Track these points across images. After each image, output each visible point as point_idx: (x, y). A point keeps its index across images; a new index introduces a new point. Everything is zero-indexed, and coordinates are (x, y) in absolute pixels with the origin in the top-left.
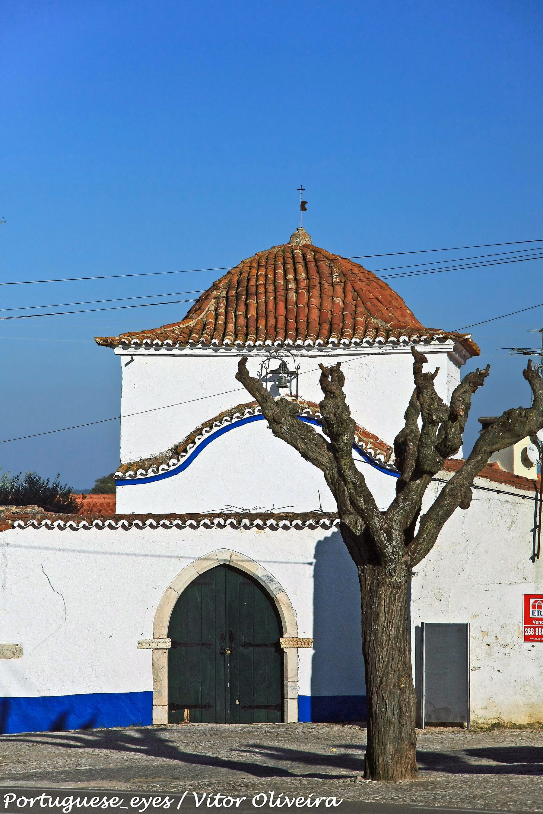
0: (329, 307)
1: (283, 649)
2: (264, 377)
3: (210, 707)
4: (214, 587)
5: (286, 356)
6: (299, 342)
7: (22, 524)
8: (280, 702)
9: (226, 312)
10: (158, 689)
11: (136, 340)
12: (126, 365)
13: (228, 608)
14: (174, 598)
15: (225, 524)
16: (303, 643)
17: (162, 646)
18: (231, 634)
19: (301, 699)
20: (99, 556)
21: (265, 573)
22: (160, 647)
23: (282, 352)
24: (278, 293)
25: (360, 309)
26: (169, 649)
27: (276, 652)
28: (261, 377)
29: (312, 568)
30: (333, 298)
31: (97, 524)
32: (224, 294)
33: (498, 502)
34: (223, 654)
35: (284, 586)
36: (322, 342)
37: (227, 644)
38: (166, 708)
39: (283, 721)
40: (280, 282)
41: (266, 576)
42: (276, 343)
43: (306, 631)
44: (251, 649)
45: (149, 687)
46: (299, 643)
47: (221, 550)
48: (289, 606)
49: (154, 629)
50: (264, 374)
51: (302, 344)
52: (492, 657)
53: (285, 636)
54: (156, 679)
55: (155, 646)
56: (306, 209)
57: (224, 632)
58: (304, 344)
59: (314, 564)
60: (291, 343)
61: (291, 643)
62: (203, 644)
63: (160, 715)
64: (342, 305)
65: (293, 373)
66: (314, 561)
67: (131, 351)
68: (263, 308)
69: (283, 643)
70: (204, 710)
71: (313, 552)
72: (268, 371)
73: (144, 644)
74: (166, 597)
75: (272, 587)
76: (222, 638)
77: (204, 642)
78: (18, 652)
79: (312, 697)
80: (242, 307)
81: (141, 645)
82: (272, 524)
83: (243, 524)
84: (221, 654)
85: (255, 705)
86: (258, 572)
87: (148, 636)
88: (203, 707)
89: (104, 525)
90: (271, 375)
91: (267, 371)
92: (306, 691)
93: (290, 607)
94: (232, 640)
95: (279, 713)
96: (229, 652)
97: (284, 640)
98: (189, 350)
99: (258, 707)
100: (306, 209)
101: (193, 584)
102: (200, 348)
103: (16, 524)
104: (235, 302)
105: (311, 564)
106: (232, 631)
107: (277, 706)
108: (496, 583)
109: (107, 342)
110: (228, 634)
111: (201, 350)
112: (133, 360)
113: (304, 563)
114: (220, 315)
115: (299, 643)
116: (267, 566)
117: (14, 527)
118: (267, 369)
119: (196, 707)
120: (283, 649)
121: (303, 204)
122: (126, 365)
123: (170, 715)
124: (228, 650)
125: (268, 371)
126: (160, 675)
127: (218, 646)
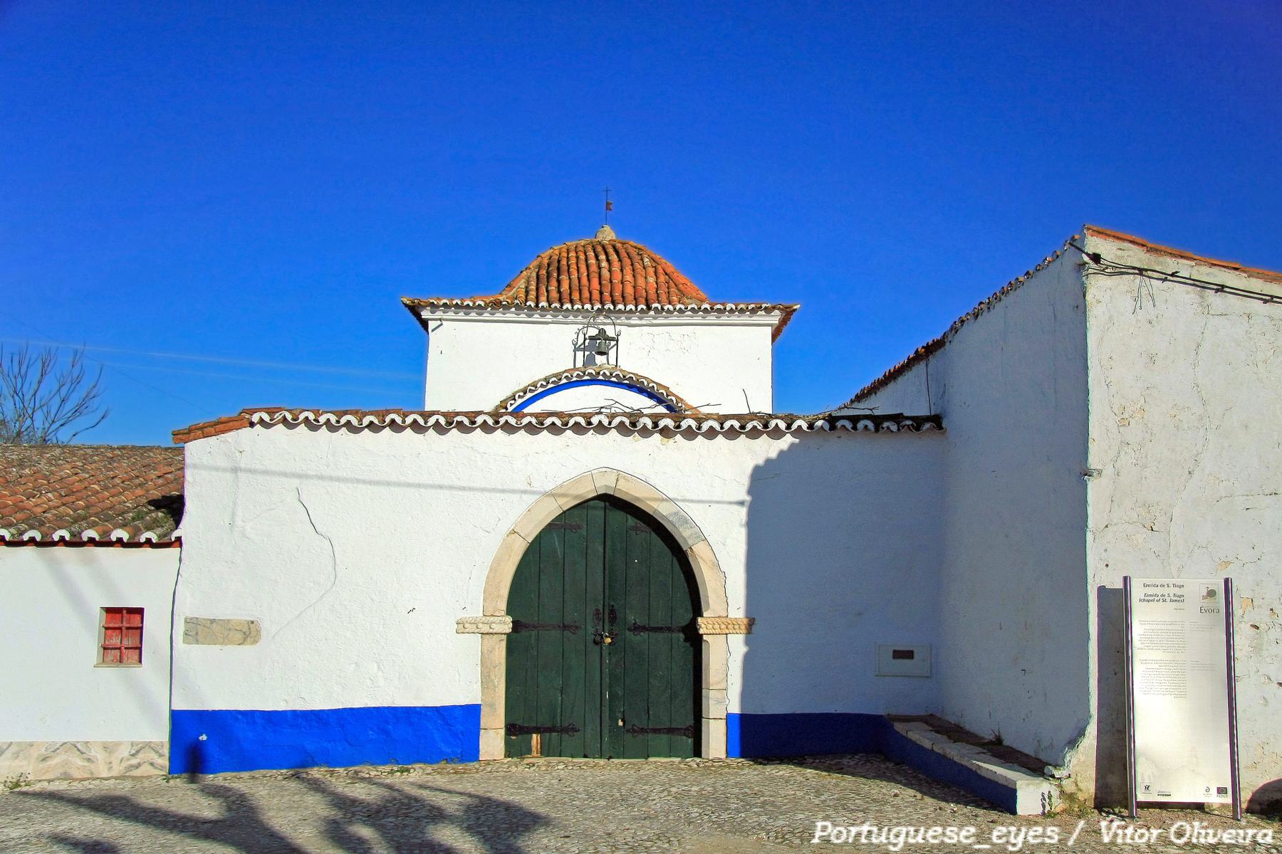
3: (575, 730)
5: (605, 324)
7: (266, 417)
8: (691, 722)
9: (537, 289)
11: (445, 301)
14: (519, 548)
17: (498, 628)
18: (612, 612)
20: (394, 478)
23: (601, 319)
25: (673, 290)
26: (508, 635)
27: (686, 640)
29: (743, 513)
31: (393, 421)
32: (534, 275)
33: (1267, 321)
34: (598, 643)
38: (503, 732)
39: (697, 752)
40: (592, 261)
41: (676, 514)
43: (737, 611)
44: (644, 635)
46: (727, 626)
50: (581, 340)
52: (1265, 653)
55: (486, 629)
59: (747, 504)
62: (565, 627)
63: (492, 741)
65: (613, 339)
66: (748, 498)
67: (439, 314)
68: (575, 282)
70: (565, 736)
71: (745, 482)
74: (506, 547)
75: (684, 534)
78: (253, 633)
81: (462, 627)
82: (690, 426)
83: (640, 426)
84: (595, 642)
86: (662, 510)
88: (563, 730)
89: (404, 422)
99: (655, 731)
101: (550, 527)
103: (255, 418)
105: (742, 503)
107: (687, 729)
108: (1267, 492)
110: (607, 612)
113: (730, 503)
115: (727, 626)
117: (252, 425)
119: (551, 730)
121: (608, 204)
123: (508, 743)
127: (591, 630)
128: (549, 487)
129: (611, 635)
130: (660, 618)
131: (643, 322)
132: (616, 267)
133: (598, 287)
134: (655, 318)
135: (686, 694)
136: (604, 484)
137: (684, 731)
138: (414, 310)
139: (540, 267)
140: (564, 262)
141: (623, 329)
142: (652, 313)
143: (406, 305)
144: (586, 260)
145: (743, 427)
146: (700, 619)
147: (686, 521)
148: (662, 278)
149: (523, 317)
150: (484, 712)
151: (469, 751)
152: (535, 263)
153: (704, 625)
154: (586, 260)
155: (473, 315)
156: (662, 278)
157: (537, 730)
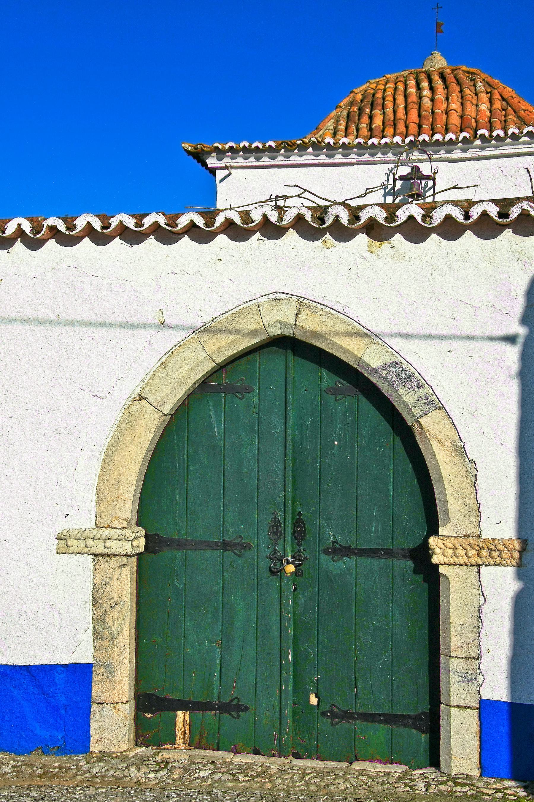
0: (474, 115)
1: (437, 566)
2: (391, 190)
4: (256, 399)
5: (420, 161)
6: (438, 137)
8: (426, 707)
10: (103, 657)
11: (231, 144)
12: (221, 181)
13: (290, 453)
15: (281, 219)
16: (495, 554)
17: (115, 547)
19: (486, 708)
21: (389, 359)
22: (110, 552)
23: (416, 155)
24: (410, 100)
25: (512, 117)
26: (139, 555)
27: (416, 571)
28: (387, 190)
29: (512, 355)
30: (477, 105)
34: (276, 572)
35: (443, 392)
36: (467, 135)
37: (288, 549)
39: (434, 761)
40: (412, 90)
41: (394, 364)
42: (407, 140)
43: (501, 522)
44: (349, 561)
45: (83, 655)
46: (488, 552)
47: (272, 297)
48: (456, 447)
49: (98, 503)
51: (441, 140)
53: (442, 531)
54: (100, 632)
55: (99, 547)
56: (442, 32)
57: (280, 515)
58: (444, 138)
60: (427, 138)
61: (461, 552)
63: (112, 724)
64: (488, 114)
65: (428, 178)
67: (227, 161)
68: (390, 116)
69: (437, 550)
70: (226, 717)
71: (518, 305)
72: (397, 177)
73: (71, 542)
74: (127, 421)
76: (276, 530)
77: (228, 539)
79: (511, 705)
80: (365, 120)
81: (64, 543)
82: (411, 218)
85: (360, 710)
86: (371, 358)
87: (84, 520)
88: (225, 708)
90: (401, 182)
91: (394, 176)
92: (497, 690)
93: (460, 449)
94: (299, 536)
95: (424, 738)
96: (291, 568)
97: (440, 543)
98: (297, 158)
100: (442, 32)
102: (310, 154)
104: (357, 117)
105: (511, 339)
106: (300, 514)
107: (417, 718)
109: (197, 148)
111: (312, 157)
112: (230, 174)
113: (492, 339)
114: (339, 131)
115: (488, 552)
116: (397, 344)
118: (394, 175)
119: (206, 706)
120: (437, 566)
121: (438, 25)
122: (221, 181)
124: (288, 563)
125: (397, 177)
126: (110, 623)
128: (198, 323)
129: (297, 561)
130: (374, 535)
131: (468, 155)
132: (440, 94)
133: (417, 120)
134: (482, 149)
135: (418, 661)
136: (277, 320)
137: (415, 722)
138: (199, 157)
139: (351, 104)
140: (379, 95)
141: (442, 166)
142: (478, 142)
143: (189, 153)
144: (406, 89)
145: (503, 215)
146: (432, 541)
147: (409, 377)
148: (498, 105)
149: (322, 159)
150: (98, 673)
151: (76, 737)
152: (346, 100)
153: (440, 550)
154: (406, 89)
155: (265, 160)
156: (498, 105)
157: (184, 706)
